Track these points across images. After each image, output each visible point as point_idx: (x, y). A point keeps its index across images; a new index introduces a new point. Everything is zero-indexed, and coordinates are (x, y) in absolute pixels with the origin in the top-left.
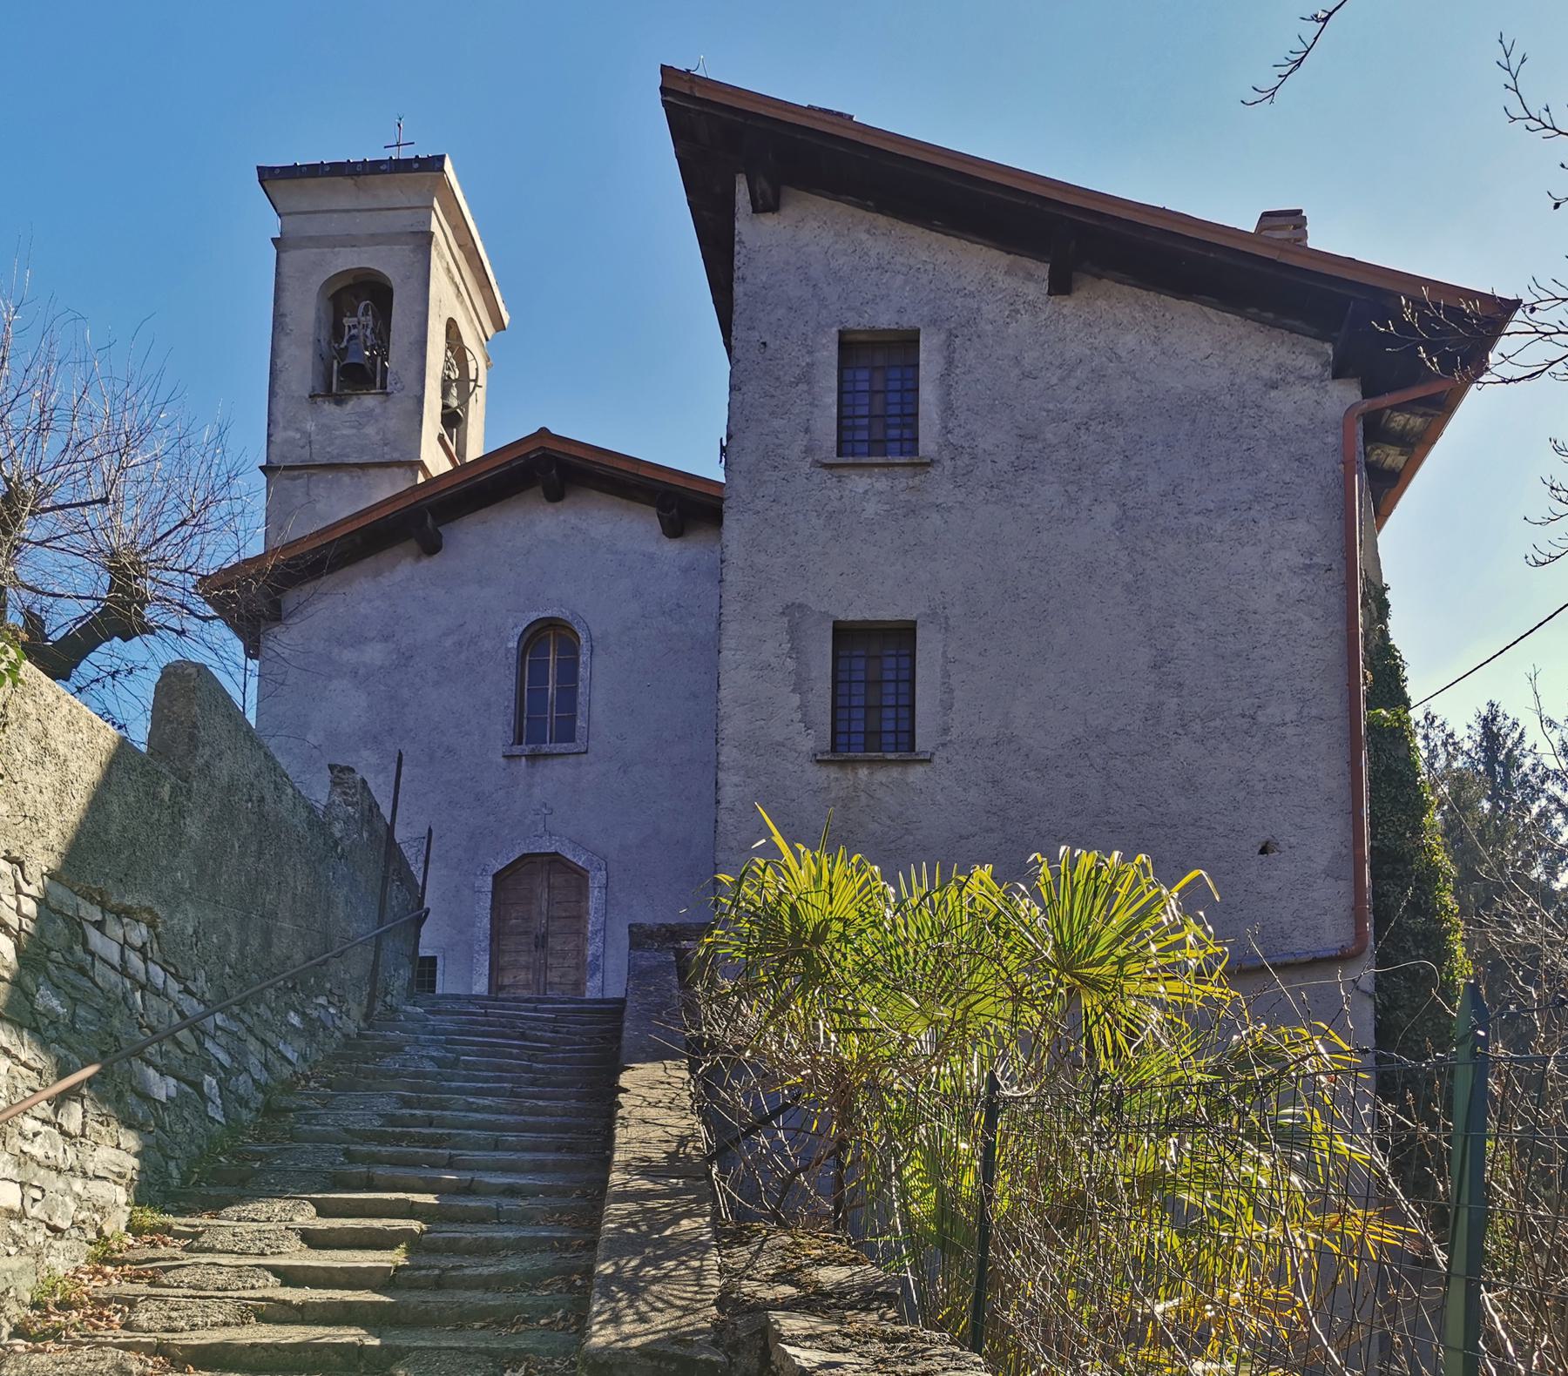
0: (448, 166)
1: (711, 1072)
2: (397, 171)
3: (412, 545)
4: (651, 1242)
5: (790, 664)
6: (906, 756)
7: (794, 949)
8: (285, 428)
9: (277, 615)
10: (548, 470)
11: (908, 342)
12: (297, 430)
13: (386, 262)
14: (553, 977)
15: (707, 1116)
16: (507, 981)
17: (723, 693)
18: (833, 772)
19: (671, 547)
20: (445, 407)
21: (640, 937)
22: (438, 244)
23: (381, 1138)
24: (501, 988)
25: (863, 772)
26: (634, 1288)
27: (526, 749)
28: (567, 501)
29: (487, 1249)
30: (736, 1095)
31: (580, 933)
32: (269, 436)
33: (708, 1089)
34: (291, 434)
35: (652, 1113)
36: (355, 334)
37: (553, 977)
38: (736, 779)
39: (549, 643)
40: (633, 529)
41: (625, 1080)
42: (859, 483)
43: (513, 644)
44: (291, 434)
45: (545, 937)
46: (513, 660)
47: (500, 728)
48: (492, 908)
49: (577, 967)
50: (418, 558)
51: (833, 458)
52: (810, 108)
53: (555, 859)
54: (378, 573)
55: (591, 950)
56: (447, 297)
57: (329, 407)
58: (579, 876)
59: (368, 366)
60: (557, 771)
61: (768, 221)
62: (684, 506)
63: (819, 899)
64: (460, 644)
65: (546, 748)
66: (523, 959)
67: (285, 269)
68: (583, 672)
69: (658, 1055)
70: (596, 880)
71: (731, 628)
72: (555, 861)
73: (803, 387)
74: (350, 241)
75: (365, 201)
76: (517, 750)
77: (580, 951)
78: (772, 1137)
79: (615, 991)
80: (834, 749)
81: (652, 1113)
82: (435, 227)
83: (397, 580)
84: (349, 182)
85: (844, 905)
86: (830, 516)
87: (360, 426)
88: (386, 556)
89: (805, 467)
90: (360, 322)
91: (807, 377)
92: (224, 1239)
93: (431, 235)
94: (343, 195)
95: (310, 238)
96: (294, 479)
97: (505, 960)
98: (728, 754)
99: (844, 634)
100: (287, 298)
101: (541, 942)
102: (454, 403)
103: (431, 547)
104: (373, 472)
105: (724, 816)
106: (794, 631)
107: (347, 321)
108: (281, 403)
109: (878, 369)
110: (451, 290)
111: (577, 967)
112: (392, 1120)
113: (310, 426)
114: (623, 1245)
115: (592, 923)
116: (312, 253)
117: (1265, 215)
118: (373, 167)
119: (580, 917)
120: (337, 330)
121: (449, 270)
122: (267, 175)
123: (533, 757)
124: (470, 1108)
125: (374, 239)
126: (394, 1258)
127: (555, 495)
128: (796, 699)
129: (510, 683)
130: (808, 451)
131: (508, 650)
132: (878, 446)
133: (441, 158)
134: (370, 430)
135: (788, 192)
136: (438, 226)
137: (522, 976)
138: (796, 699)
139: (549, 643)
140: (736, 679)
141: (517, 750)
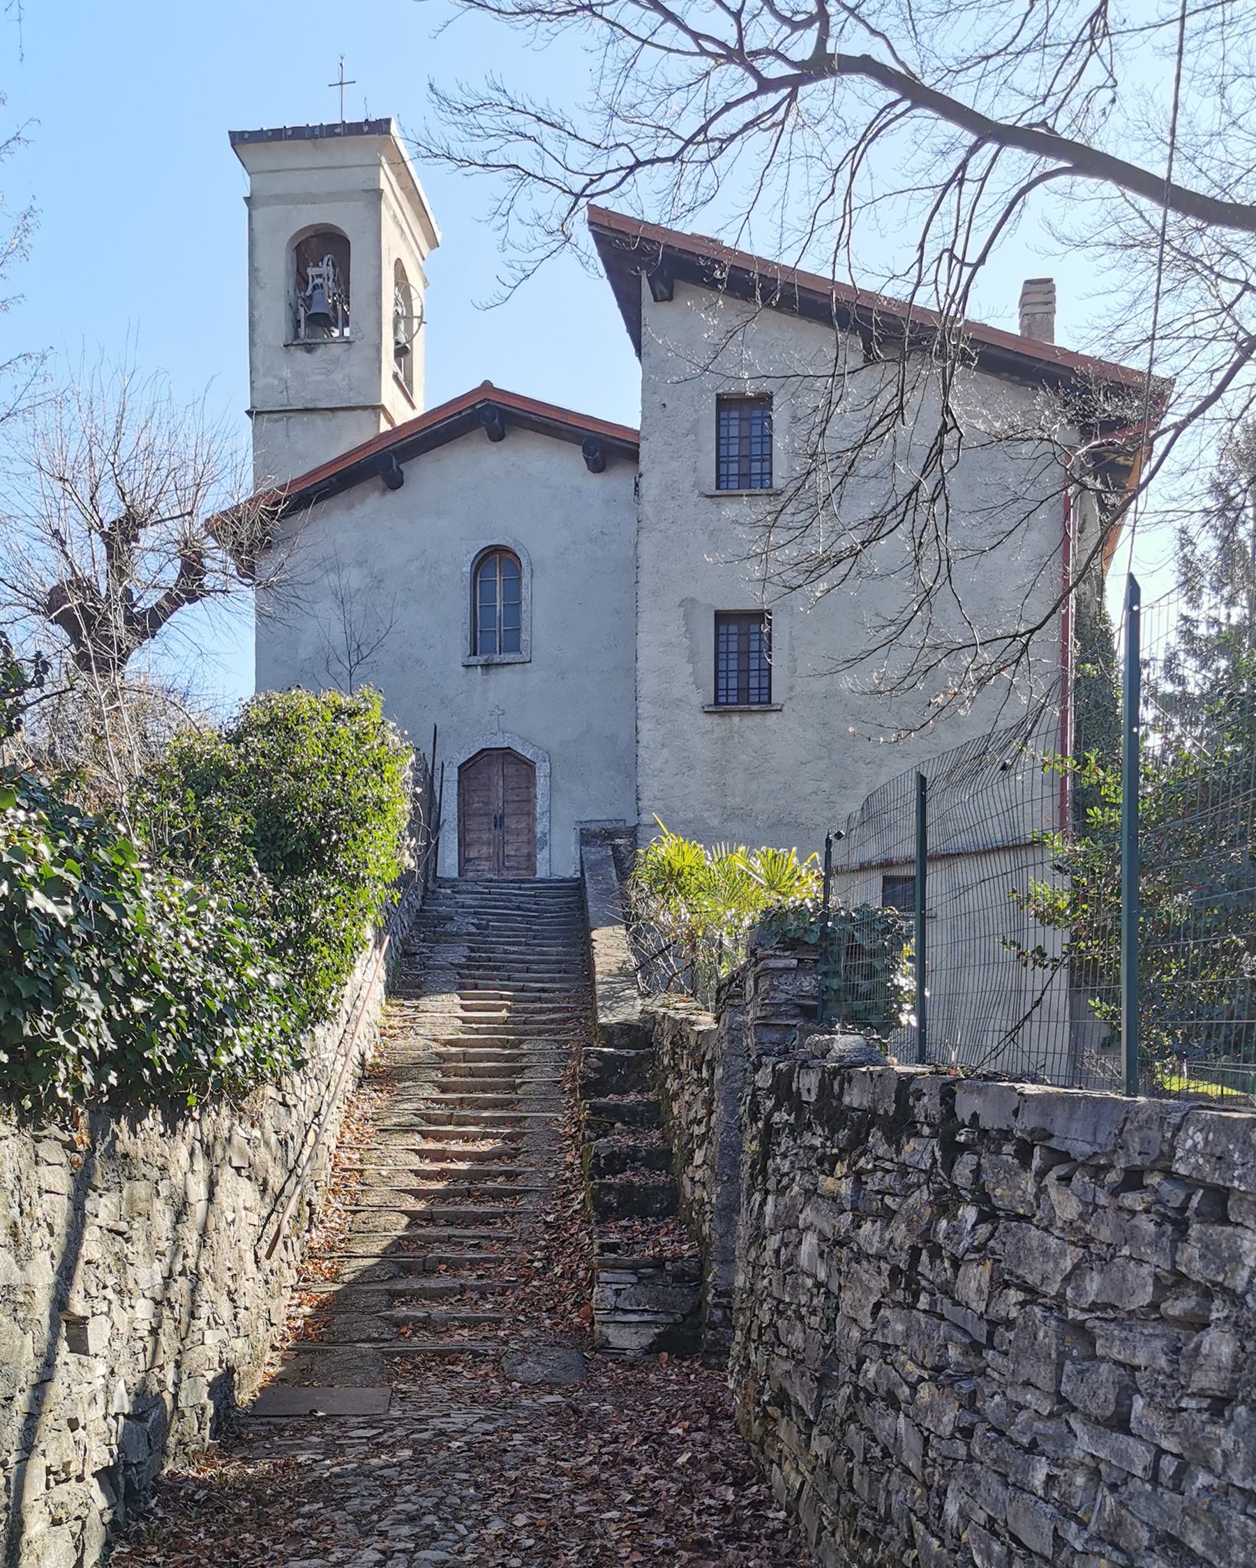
0: (394, 128)
1: (636, 931)
2: (350, 133)
3: (378, 480)
4: (614, 996)
5: (686, 642)
6: (764, 707)
7: (670, 880)
8: (265, 375)
9: (267, 545)
10: (491, 416)
11: (764, 400)
12: (275, 377)
13: (342, 218)
14: (510, 850)
15: (634, 951)
16: (472, 855)
17: (639, 664)
18: (715, 719)
19: (596, 481)
20: (397, 343)
21: (587, 837)
22: (389, 207)
23: (468, 967)
24: (468, 860)
25: (736, 719)
26: (611, 1009)
27: (481, 659)
28: (505, 441)
29: (541, 1011)
30: (649, 942)
31: (530, 814)
32: (252, 382)
33: (636, 936)
34: (270, 380)
35: (609, 951)
36: (318, 281)
37: (510, 850)
38: (649, 726)
39: (496, 564)
40: (567, 463)
41: (594, 935)
42: (730, 510)
43: (467, 569)
44: (270, 380)
45: (502, 818)
46: (467, 582)
47: (459, 641)
48: (459, 795)
49: (529, 842)
50: (384, 493)
51: (713, 491)
52: (693, 235)
53: (507, 752)
54: (351, 507)
55: (539, 829)
56: (397, 241)
57: (301, 355)
58: (529, 766)
59: (331, 314)
60: (505, 679)
61: (664, 306)
62: (607, 449)
63: (680, 858)
64: (423, 569)
65: (497, 658)
66: (485, 836)
67: (256, 226)
68: (525, 593)
69: (611, 922)
70: (542, 770)
71: (645, 617)
72: (507, 754)
73: (691, 437)
74: (310, 198)
75: (323, 160)
76: (473, 660)
77: (531, 830)
78: (666, 960)
79: (569, 870)
80: (717, 703)
81: (609, 951)
82: (384, 185)
83: (369, 510)
84: (308, 143)
85: (690, 859)
86: (711, 534)
87: (328, 372)
88: (356, 491)
89: (694, 497)
90: (323, 270)
91: (693, 430)
92: (429, 1007)
93: (379, 193)
94: (300, 155)
95: (276, 196)
96: (276, 421)
97: (470, 837)
98: (644, 708)
99: (721, 618)
100: (259, 251)
101: (499, 822)
102: (403, 340)
103: (395, 483)
104: (341, 414)
105: (641, 752)
106: (687, 616)
107: (311, 271)
108: (259, 350)
109: (743, 416)
110: (397, 231)
111: (529, 842)
112: (469, 958)
113: (286, 373)
114: (604, 998)
115: (541, 805)
116: (279, 209)
117: (1027, 282)
118: (329, 131)
119: (530, 800)
120: (301, 280)
121: (395, 216)
122: (239, 139)
123: (487, 666)
124: (506, 952)
125: (333, 196)
126: (504, 1013)
127: (497, 436)
128: (690, 668)
129: (466, 603)
130: (695, 485)
131: (463, 574)
132: (746, 480)
133: (388, 121)
134: (337, 376)
135: (680, 285)
136: (387, 180)
137: (485, 850)
138: (690, 668)
139: (496, 564)
140: (649, 652)
141: (473, 660)
